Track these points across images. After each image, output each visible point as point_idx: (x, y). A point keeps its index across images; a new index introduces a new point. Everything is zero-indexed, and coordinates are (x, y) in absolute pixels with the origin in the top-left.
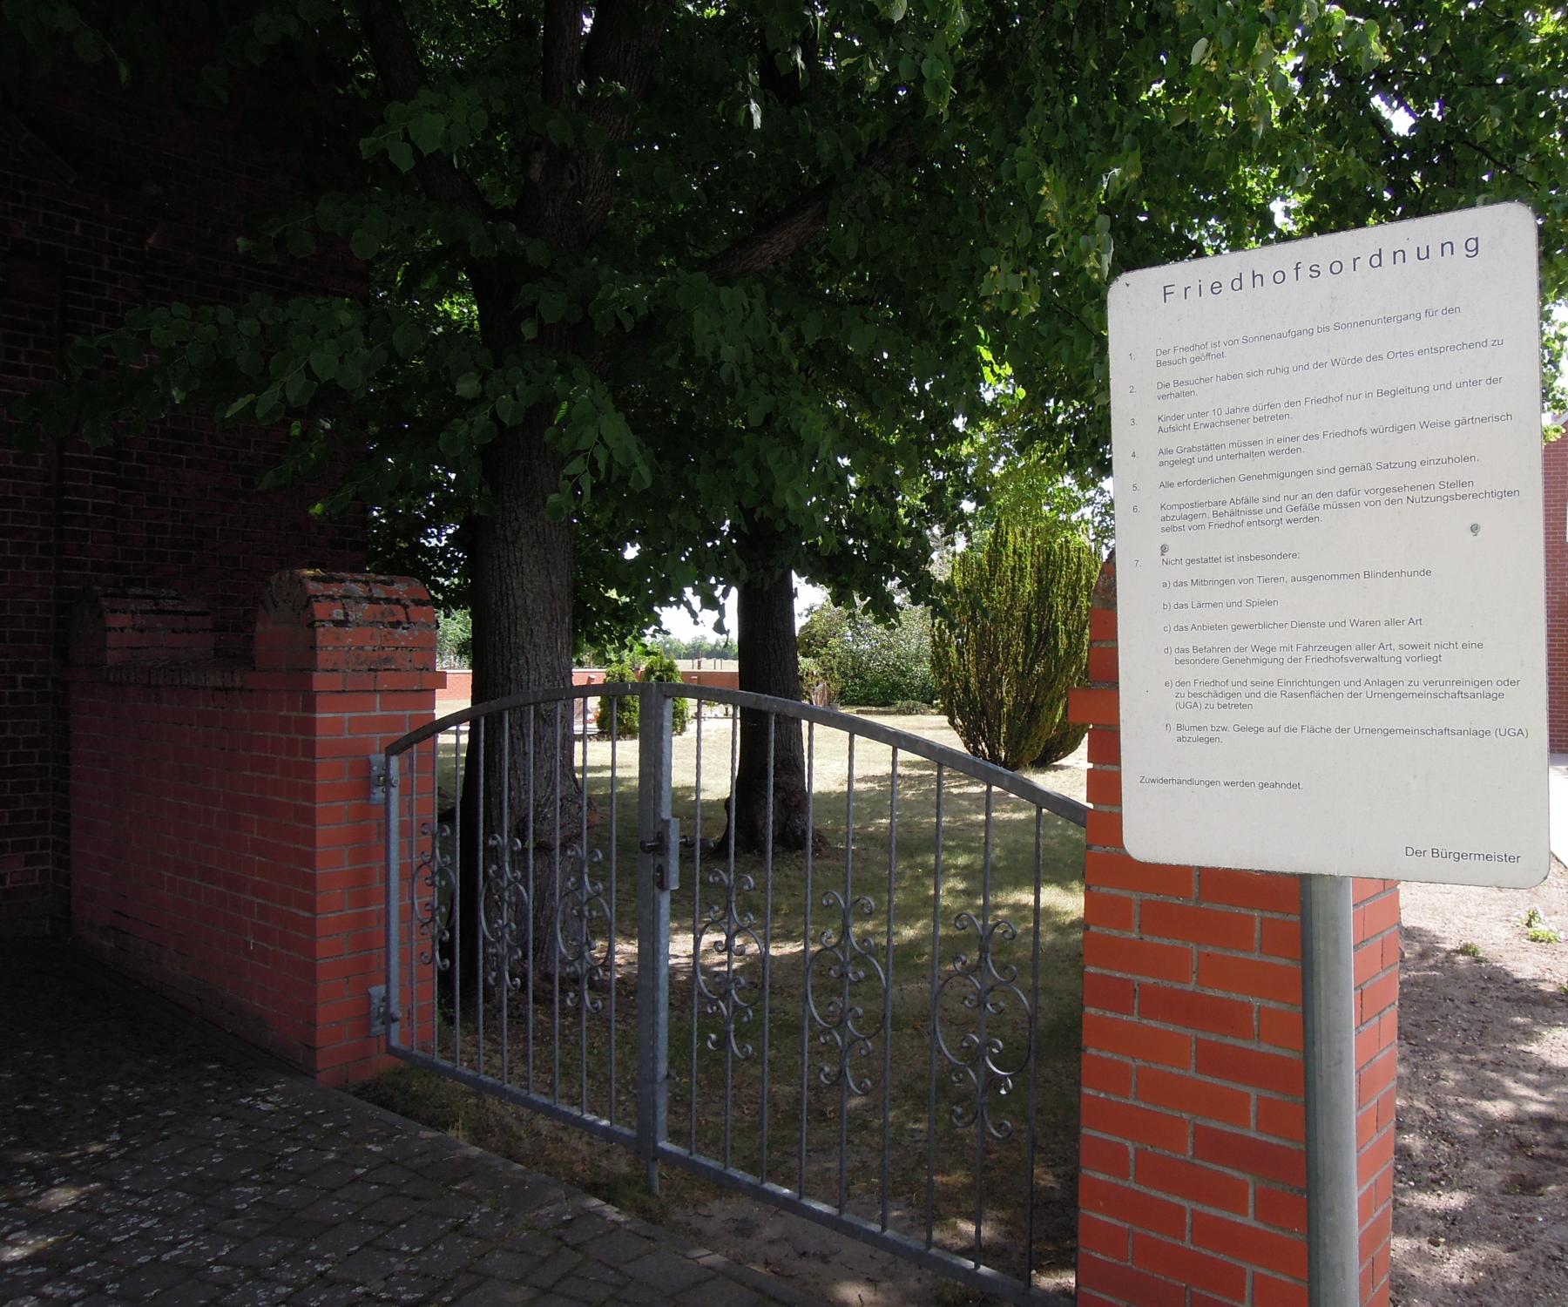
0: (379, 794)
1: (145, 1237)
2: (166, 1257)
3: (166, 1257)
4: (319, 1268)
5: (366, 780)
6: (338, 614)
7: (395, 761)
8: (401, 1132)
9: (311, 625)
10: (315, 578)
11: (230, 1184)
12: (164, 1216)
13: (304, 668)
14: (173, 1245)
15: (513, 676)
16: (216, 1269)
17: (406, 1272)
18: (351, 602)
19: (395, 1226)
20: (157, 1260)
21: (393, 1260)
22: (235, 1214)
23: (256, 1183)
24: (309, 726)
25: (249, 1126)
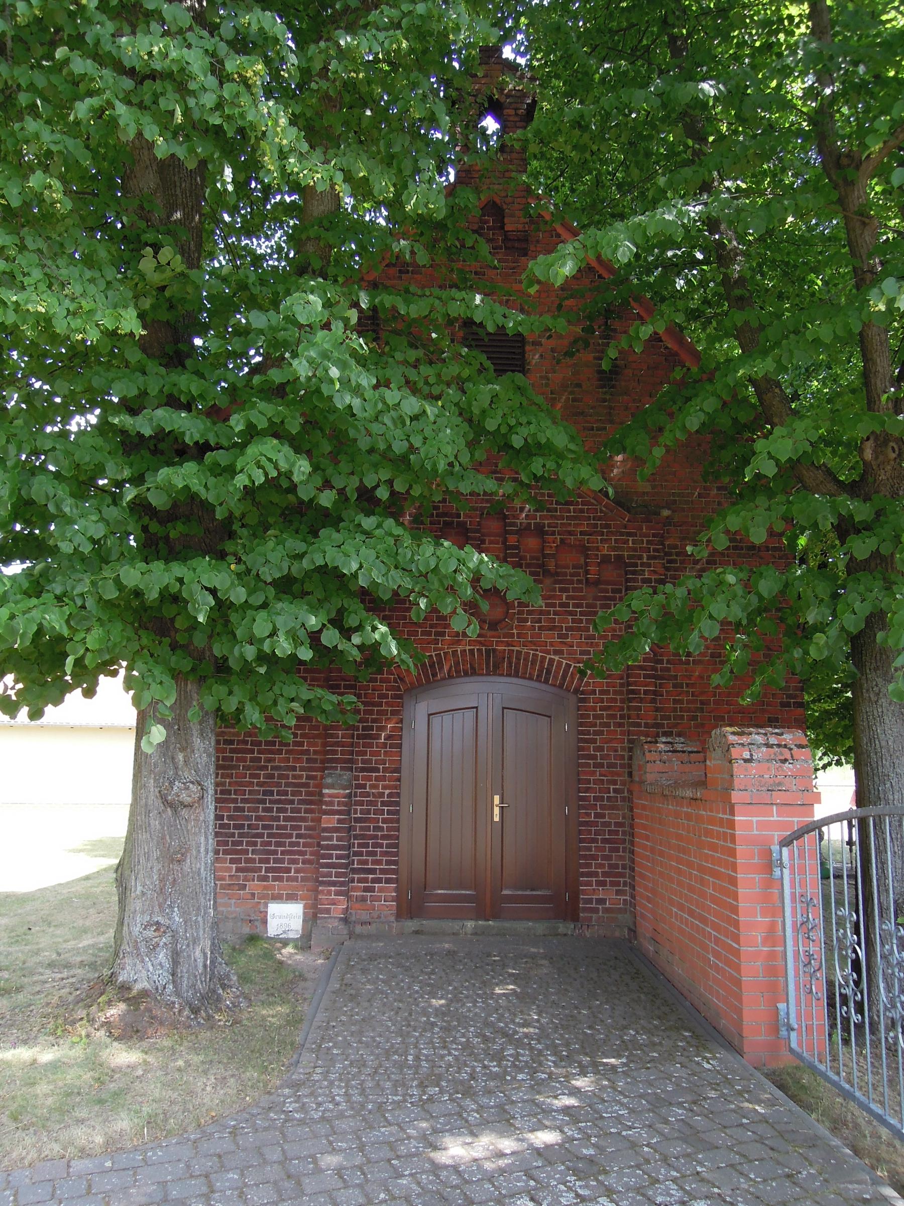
0: (777, 872)
1: (619, 1119)
2: (624, 1133)
3: (624, 1133)
4: (699, 1169)
5: (769, 864)
6: (746, 755)
7: (785, 851)
8: (781, 1105)
9: (730, 762)
10: (733, 733)
11: (670, 1104)
12: (632, 1111)
13: (729, 787)
14: (630, 1128)
15: (882, 796)
16: (646, 1149)
17: (748, 1191)
18: (755, 747)
19: (751, 1161)
20: (619, 1134)
21: (742, 1180)
22: (666, 1122)
23: (685, 1108)
24: (731, 824)
25: (694, 1074)
